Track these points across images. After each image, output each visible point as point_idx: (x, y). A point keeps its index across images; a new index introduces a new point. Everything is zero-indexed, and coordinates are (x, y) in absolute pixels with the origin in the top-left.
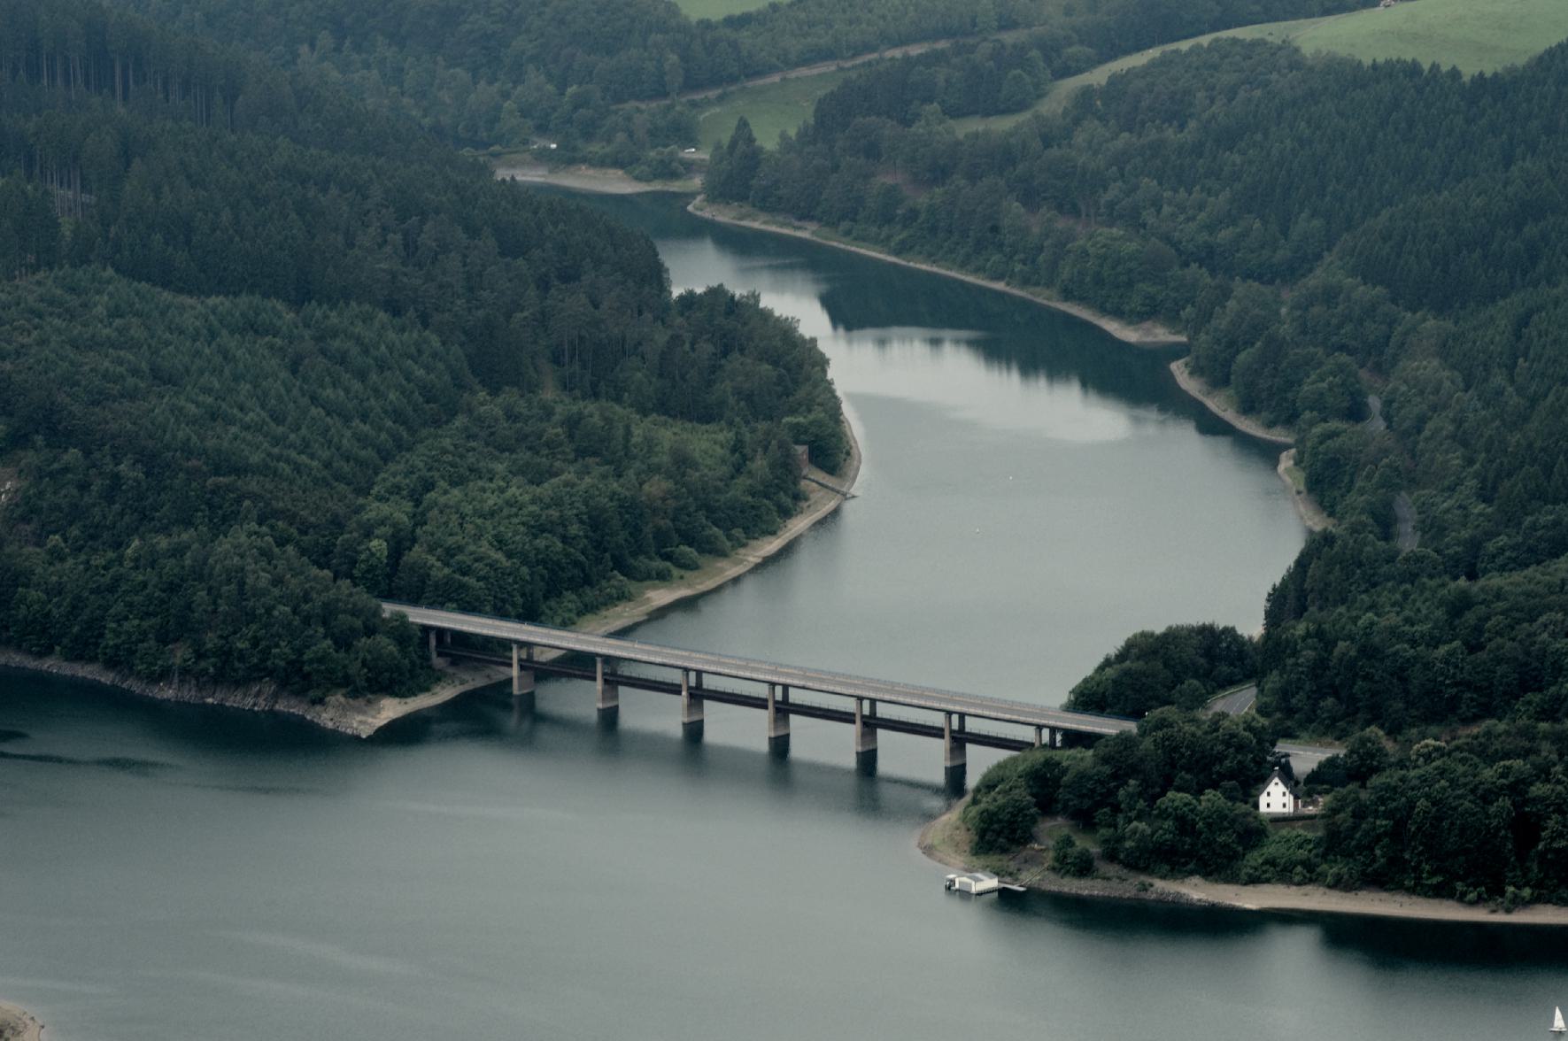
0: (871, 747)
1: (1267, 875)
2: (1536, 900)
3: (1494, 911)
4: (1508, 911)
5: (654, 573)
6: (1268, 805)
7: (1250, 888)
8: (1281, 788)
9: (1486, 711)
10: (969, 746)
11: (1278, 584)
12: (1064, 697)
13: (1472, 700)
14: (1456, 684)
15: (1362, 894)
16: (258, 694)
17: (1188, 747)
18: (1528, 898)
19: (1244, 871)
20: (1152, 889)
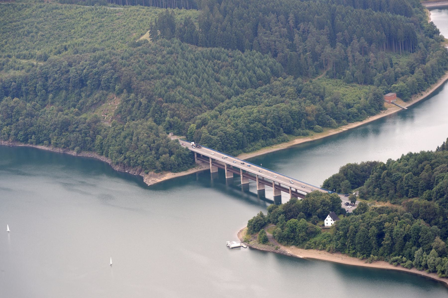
0: (279, 195)
1: (312, 247)
2: (378, 260)
3: (366, 263)
4: (371, 263)
5: (301, 134)
6: (327, 223)
7: (307, 250)
8: (330, 218)
9: (416, 195)
10: (273, 199)
11: (440, 147)
12: (322, 184)
13: (412, 191)
14: (408, 186)
15: (335, 255)
16: (136, 170)
17: (311, 204)
18: (375, 259)
19: (306, 245)
20: (279, 249)
